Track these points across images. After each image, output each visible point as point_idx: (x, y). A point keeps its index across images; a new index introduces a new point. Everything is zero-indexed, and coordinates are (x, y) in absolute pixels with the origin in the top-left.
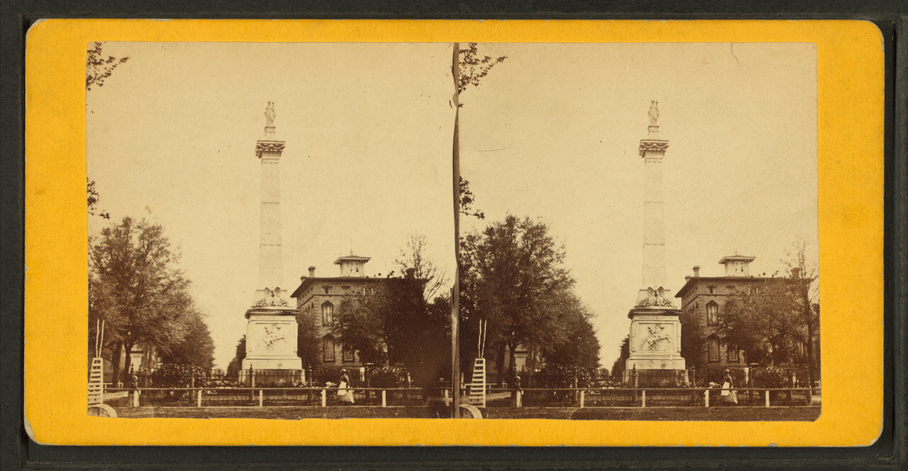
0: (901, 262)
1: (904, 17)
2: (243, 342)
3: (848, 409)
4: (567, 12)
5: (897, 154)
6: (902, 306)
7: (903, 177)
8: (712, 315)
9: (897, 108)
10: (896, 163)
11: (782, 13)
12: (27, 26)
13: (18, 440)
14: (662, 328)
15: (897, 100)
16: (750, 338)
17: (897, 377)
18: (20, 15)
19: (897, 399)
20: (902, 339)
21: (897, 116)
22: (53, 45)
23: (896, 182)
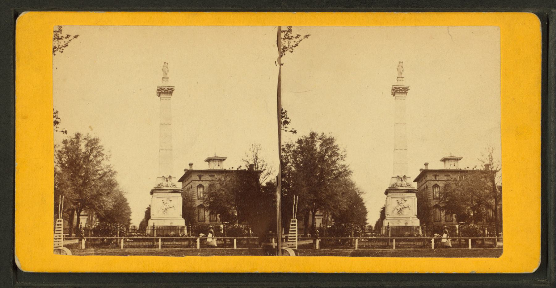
0: (552, 160)
1: (553, 10)
3: (519, 250)
4: (347, 7)
5: (549, 94)
9: (549, 66)
11: (479, 8)
12: (16, 16)
13: (11, 269)
15: (549, 61)
16: (459, 207)
17: (549, 231)
18: (12, 9)
19: (549, 244)
20: (552, 207)
21: (549, 71)
22: (32, 28)
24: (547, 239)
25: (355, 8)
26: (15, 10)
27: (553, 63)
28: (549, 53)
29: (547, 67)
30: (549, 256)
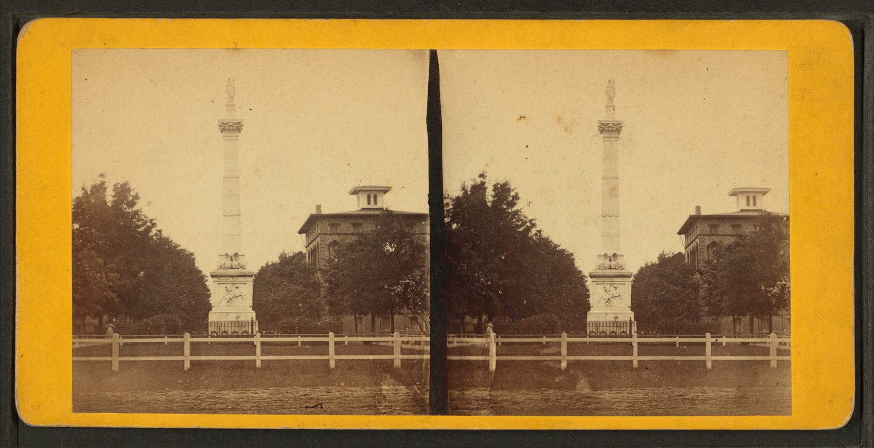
0: (868, 304)
1: (871, 16)
2: (434, 55)
3: (817, 386)
4: (543, 11)
5: (865, 151)
6: (869, 428)
7: (871, 343)
8: (654, 393)
9: (865, 105)
10: (864, 161)
12: (17, 30)
13: (9, 406)
14: (237, 288)
15: (865, 98)
16: (725, 279)
17: (865, 367)
18: (10, 14)
19: (865, 388)
20: (870, 330)
21: (865, 114)
22: (42, 42)
23: (864, 177)
24: (862, 121)
25: (556, 13)
26: (14, 17)
27: (871, 100)
28: (865, 85)
29: (862, 106)
30: (864, 407)
